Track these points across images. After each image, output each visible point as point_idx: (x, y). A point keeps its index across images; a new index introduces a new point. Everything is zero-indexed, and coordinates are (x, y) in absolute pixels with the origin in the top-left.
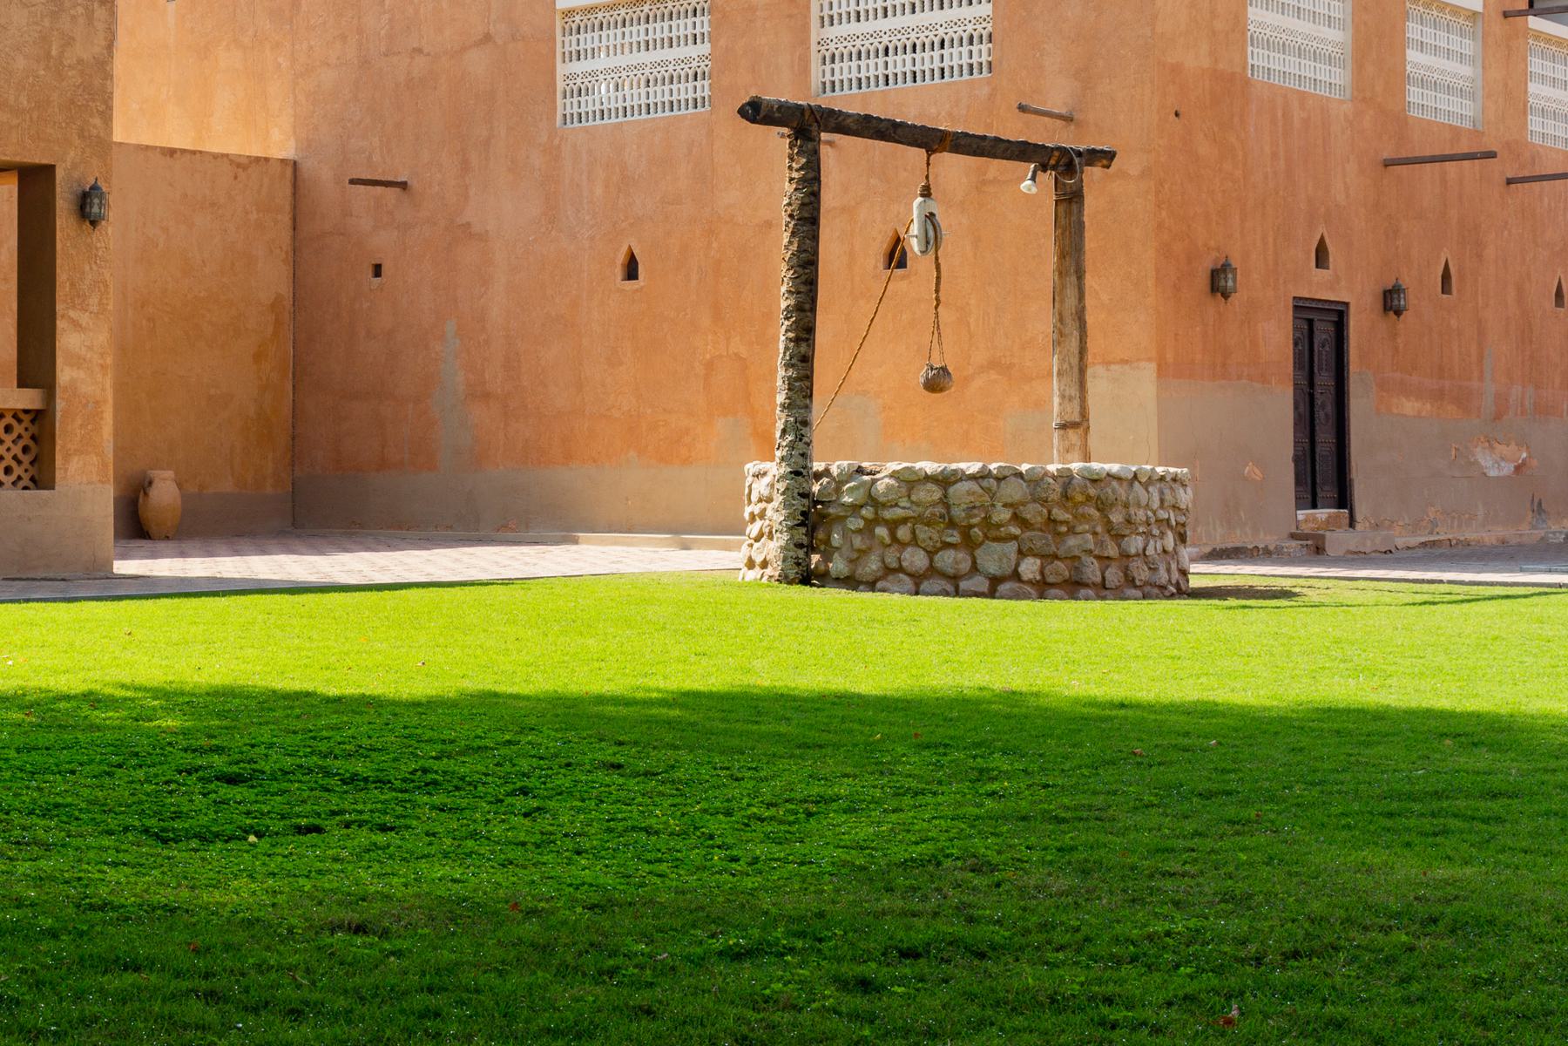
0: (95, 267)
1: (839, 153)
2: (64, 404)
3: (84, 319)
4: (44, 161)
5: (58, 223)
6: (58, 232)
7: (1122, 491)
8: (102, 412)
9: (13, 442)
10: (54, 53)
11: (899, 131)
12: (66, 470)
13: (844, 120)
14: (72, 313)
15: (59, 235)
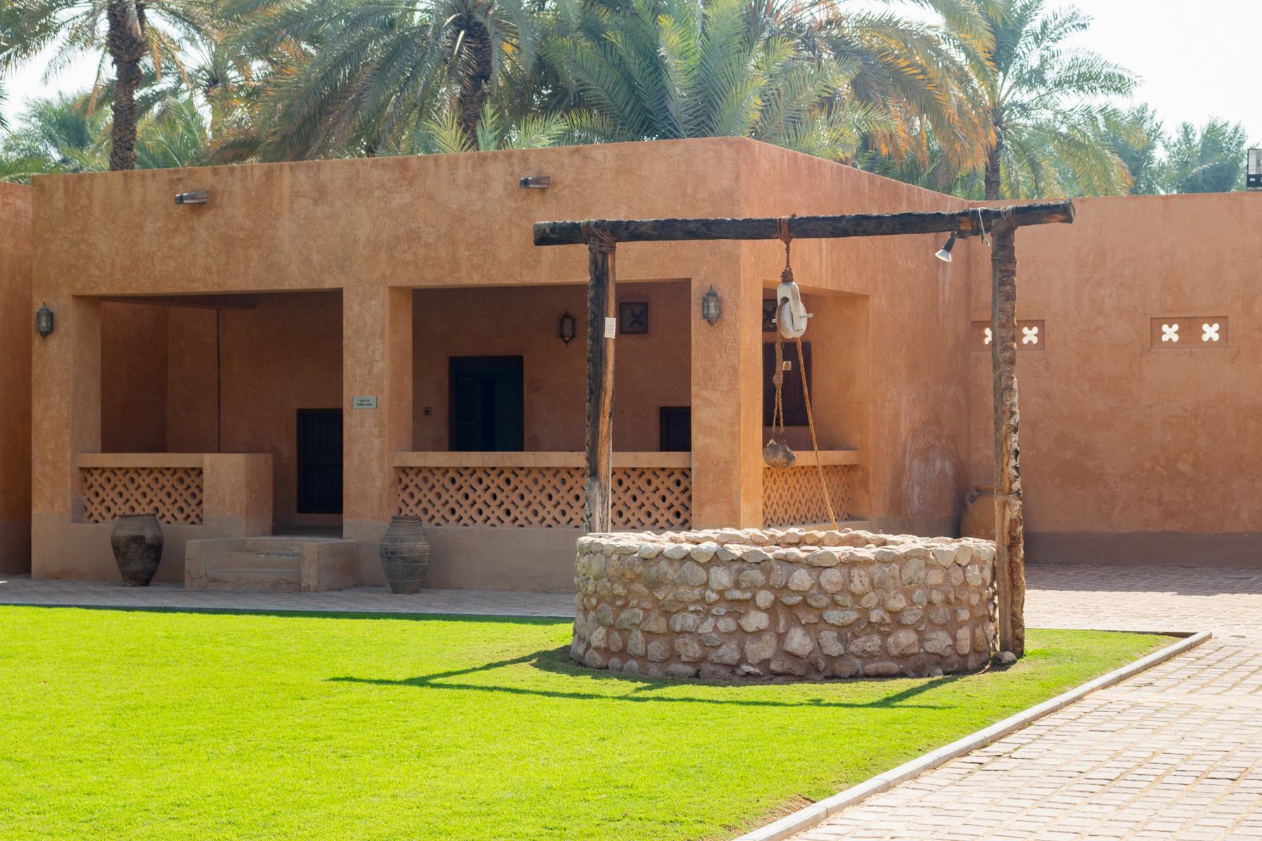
0: (724, 355)
1: (1024, 236)
2: (698, 463)
3: (715, 397)
4: (682, 276)
5: (693, 323)
6: (693, 331)
7: (670, 572)
8: (731, 470)
9: (489, 488)
10: (689, 191)
11: (830, 229)
12: (700, 516)
13: (637, 228)
14: (704, 393)
15: (693, 331)
